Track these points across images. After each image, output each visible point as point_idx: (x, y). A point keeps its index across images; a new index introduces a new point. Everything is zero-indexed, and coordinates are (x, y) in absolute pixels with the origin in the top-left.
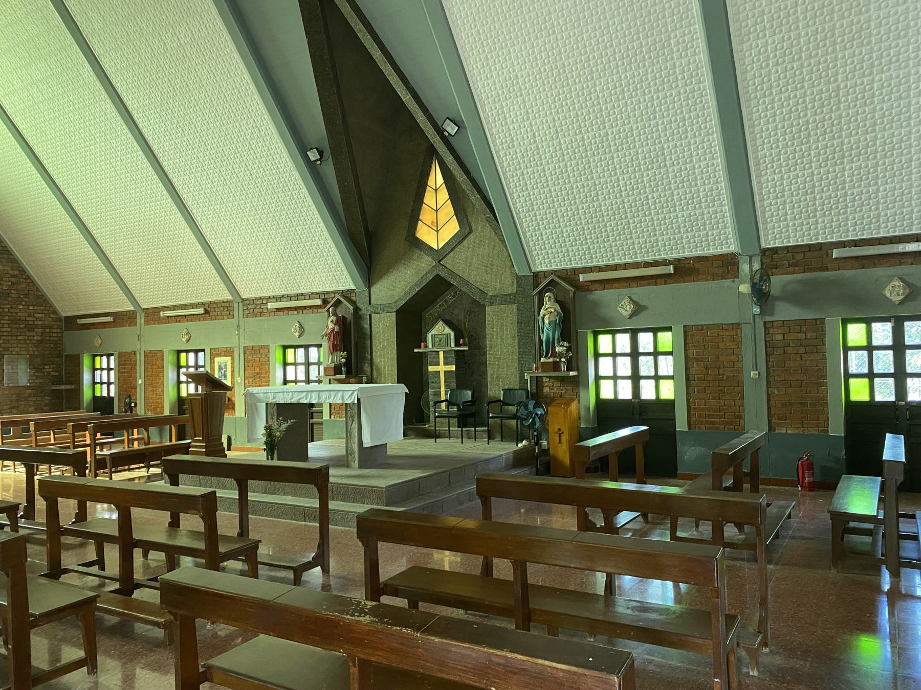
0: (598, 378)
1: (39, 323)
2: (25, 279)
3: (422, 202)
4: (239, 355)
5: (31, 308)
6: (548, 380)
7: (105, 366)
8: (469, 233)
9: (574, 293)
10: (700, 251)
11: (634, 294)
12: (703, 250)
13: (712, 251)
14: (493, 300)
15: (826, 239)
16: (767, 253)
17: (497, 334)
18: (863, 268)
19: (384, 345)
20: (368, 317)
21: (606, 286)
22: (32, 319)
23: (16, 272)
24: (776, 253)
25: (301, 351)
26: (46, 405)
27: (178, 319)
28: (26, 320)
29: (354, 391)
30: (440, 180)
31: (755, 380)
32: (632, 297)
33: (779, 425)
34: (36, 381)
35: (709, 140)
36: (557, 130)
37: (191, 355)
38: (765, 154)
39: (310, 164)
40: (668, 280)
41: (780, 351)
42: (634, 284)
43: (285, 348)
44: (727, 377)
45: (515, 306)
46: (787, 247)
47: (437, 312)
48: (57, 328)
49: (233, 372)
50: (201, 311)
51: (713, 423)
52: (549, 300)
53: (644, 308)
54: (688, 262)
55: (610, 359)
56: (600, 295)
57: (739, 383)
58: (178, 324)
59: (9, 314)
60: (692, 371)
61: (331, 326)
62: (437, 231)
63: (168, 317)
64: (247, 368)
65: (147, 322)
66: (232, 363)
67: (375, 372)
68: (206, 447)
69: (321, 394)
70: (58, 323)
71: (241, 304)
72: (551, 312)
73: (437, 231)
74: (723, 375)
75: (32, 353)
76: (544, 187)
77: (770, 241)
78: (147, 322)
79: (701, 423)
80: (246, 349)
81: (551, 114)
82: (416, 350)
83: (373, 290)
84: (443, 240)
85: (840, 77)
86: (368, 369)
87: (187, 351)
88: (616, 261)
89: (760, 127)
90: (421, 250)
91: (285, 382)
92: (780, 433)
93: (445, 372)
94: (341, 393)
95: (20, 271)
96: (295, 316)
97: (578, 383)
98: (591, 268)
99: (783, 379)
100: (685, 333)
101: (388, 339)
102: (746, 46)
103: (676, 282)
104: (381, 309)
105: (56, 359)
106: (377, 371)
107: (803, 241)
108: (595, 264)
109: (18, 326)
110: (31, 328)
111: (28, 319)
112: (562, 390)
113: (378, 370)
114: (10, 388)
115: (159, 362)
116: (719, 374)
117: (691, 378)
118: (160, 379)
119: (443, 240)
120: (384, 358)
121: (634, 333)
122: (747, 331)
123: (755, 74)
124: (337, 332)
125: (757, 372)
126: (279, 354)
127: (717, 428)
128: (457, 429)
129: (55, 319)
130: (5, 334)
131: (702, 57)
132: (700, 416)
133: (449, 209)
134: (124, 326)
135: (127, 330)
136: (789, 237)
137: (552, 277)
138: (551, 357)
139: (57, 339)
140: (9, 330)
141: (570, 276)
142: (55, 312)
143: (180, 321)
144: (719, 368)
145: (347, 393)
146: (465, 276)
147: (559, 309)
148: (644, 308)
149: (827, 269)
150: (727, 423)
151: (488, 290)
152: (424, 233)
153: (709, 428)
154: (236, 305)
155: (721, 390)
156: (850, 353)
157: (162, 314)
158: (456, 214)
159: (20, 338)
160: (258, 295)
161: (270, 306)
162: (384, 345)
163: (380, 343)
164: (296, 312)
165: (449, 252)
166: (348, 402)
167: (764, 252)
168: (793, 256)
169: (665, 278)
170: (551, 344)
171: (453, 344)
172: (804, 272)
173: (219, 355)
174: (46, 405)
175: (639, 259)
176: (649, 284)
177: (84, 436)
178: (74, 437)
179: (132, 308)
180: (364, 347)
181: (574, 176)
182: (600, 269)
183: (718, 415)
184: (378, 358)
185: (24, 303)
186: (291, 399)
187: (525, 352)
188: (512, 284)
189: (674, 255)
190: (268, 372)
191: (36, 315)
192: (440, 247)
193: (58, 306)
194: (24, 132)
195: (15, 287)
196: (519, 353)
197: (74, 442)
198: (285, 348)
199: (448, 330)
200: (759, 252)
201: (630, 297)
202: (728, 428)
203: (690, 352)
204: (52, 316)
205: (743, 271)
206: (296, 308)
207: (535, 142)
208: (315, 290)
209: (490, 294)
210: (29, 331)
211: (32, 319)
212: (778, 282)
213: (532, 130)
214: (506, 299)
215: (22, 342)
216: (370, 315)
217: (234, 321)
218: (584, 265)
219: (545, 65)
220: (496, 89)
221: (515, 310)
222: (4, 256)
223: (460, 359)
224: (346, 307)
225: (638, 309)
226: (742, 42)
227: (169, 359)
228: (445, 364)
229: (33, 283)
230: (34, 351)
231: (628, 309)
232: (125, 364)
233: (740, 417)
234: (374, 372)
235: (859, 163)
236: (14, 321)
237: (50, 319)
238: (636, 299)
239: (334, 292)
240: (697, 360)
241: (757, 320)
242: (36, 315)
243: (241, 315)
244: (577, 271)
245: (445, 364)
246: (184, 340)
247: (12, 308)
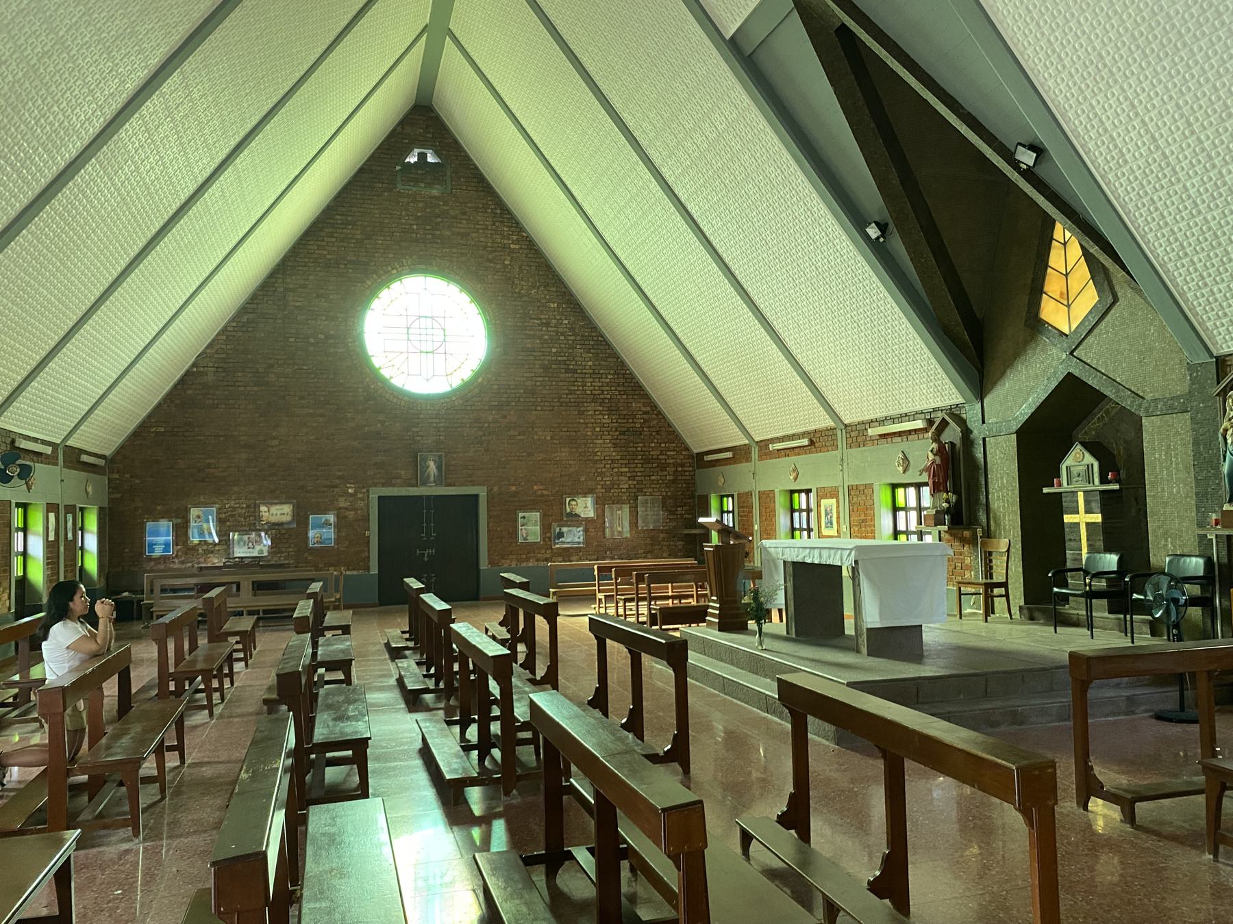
1: (671, 461)
2: (657, 415)
3: (1046, 266)
4: (843, 494)
5: (663, 445)
7: (912, 503)
19: (1002, 483)
20: (981, 442)
23: (649, 409)
26: (680, 550)
28: (658, 459)
29: (851, 550)
34: (669, 524)
36: (1188, 121)
37: (912, 491)
39: (875, 246)
43: (894, 487)
45: (1187, 416)
48: (690, 466)
49: (838, 518)
50: (805, 442)
58: (787, 458)
59: (642, 453)
61: (931, 457)
63: (778, 450)
64: (851, 513)
65: (761, 458)
66: (838, 507)
68: (720, 609)
70: (690, 461)
71: (844, 431)
73: (1069, 306)
75: (664, 494)
76: (1194, 216)
78: (761, 458)
80: (850, 488)
81: (1171, 98)
82: (1045, 490)
83: (986, 401)
87: (799, 491)
91: (896, 533)
93: (1088, 524)
94: (839, 552)
95: (651, 407)
96: (900, 445)
105: (689, 501)
106: (995, 521)
109: (650, 466)
110: (663, 467)
111: (660, 457)
114: (644, 531)
115: (772, 505)
118: (773, 525)
119: (1076, 318)
120: (1003, 501)
128: (1106, 614)
129: (687, 457)
130: (639, 474)
134: (742, 462)
135: (743, 467)
139: (690, 478)
140: (642, 470)
142: (687, 449)
143: (788, 456)
151: (1144, 391)
152: (1051, 312)
157: (771, 447)
158: (1092, 278)
159: (653, 478)
160: (861, 419)
161: (871, 432)
162: (1002, 483)
163: (997, 481)
164: (899, 439)
171: (1097, 481)
173: (825, 497)
174: (680, 550)
178: (650, 588)
179: (747, 442)
180: (977, 484)
185: (656, 441)
186: (797, 557)
187: (1207, 493)
190: (873, 519)
191: (668, 453)
195: (647, 424)
196: (1197, 494)
198: (894, 487)
199: (1089, 459)
204: (684, 453)
206: (900, 434)
207: (1158, 147)
209: (1149, 397)
213: (1147, 131)
214: (1174, 406)
215: (655, 482)
216: (984, 439)
217: (837, 453)
220: (1075, 84)
221: (1189, 422)
222: (636, 392)
223: (1108, 503)
224: (954, 430)
227: (781, 502)
237: (682, 457)
242: (668, 453)
246: (792, 477)
247: (645, 446)
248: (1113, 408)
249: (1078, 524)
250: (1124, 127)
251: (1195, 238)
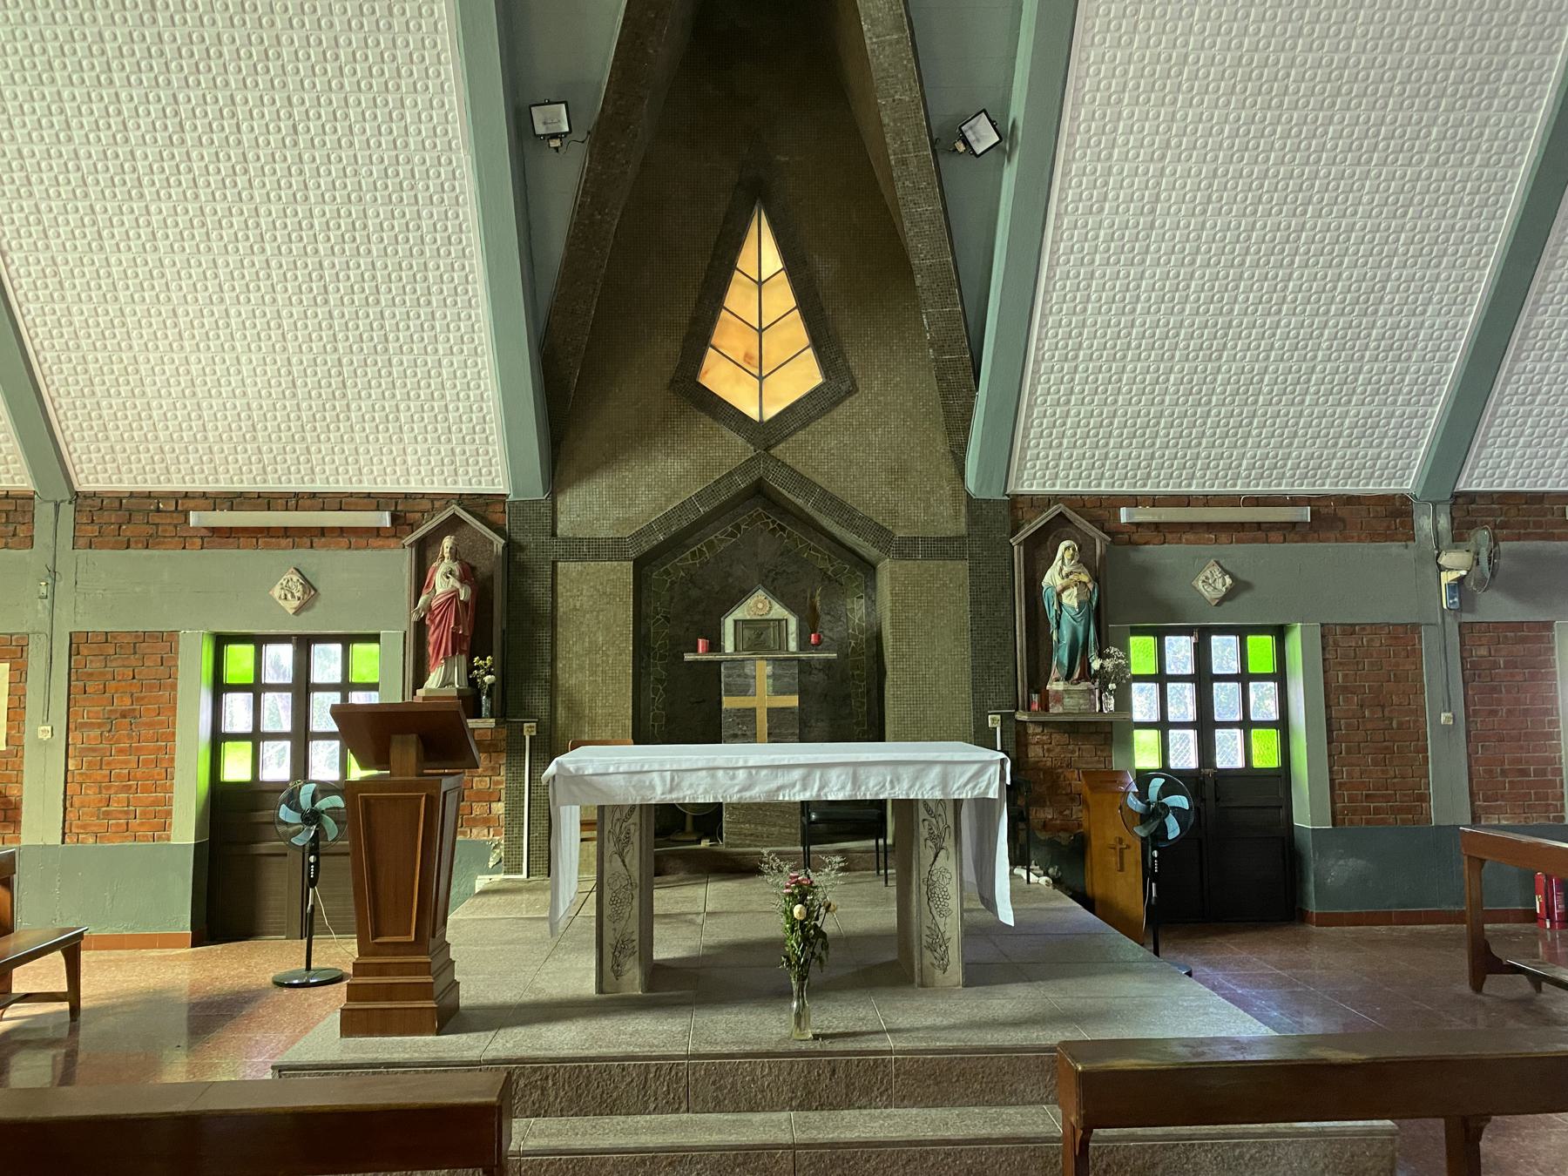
6: (1039, 730)
8: (849, 393)
13: (1372, 488)
14: (906, 549)
15: (1535, 486)
20: (548, 568)
24: (1473, 502)
29: (991, 762)
30: (772, 261)
31: (1447, 729)
32: (1221, 562)
33: (1487, 810)
43: (221, 641)
51: (1377, 811)
55: (1235, 687)
62: (761, 378)
67: (561, 712)
69: (862, 771)
71: (68, 510)
73: (761, 378)
74: (1391, 719)
79: (1354, 811)
80: (77, 643)
82: (689, 657)
83: (560, 499)
84: (777, 401)
88: (1057, 488)
90: (715, 418)
94: (937, 770)
101: (608, 629)
104: (591, 549)
112: (1073, 752)
113: (573, 707)
117: (1335, 726)
119: (777, 401)
121: (304, 644)
122: (1428, 643)
124: (465, 604)
125: (1450, 714)
127: (1383, 822)
133: (795, 332)
137: (1061, 507)
138: (1078, 681)
144: (1383, 707)
145: (958, 769)
146: (833, 489)
150: (1400, 810)
154: (43, 512)
155: (1387, 748)
165: (795, 430)
166: (966, 794)
167: (1457, 496)
169: (1289, 530)
183: (1383, 796)
188: (956, 517)
192: (767, 417)
198: (221, 641)
205: (1421, 529)
209: (900, 534)
216: (554, 564)
217: (34, 558)
231: (1219, 585)
239: (446, 498)
240: (1345, 689)
241: (1448, 619)
248: (722, 541)
249: (754, 710)
250: (227, 206)
251: (62, 376)
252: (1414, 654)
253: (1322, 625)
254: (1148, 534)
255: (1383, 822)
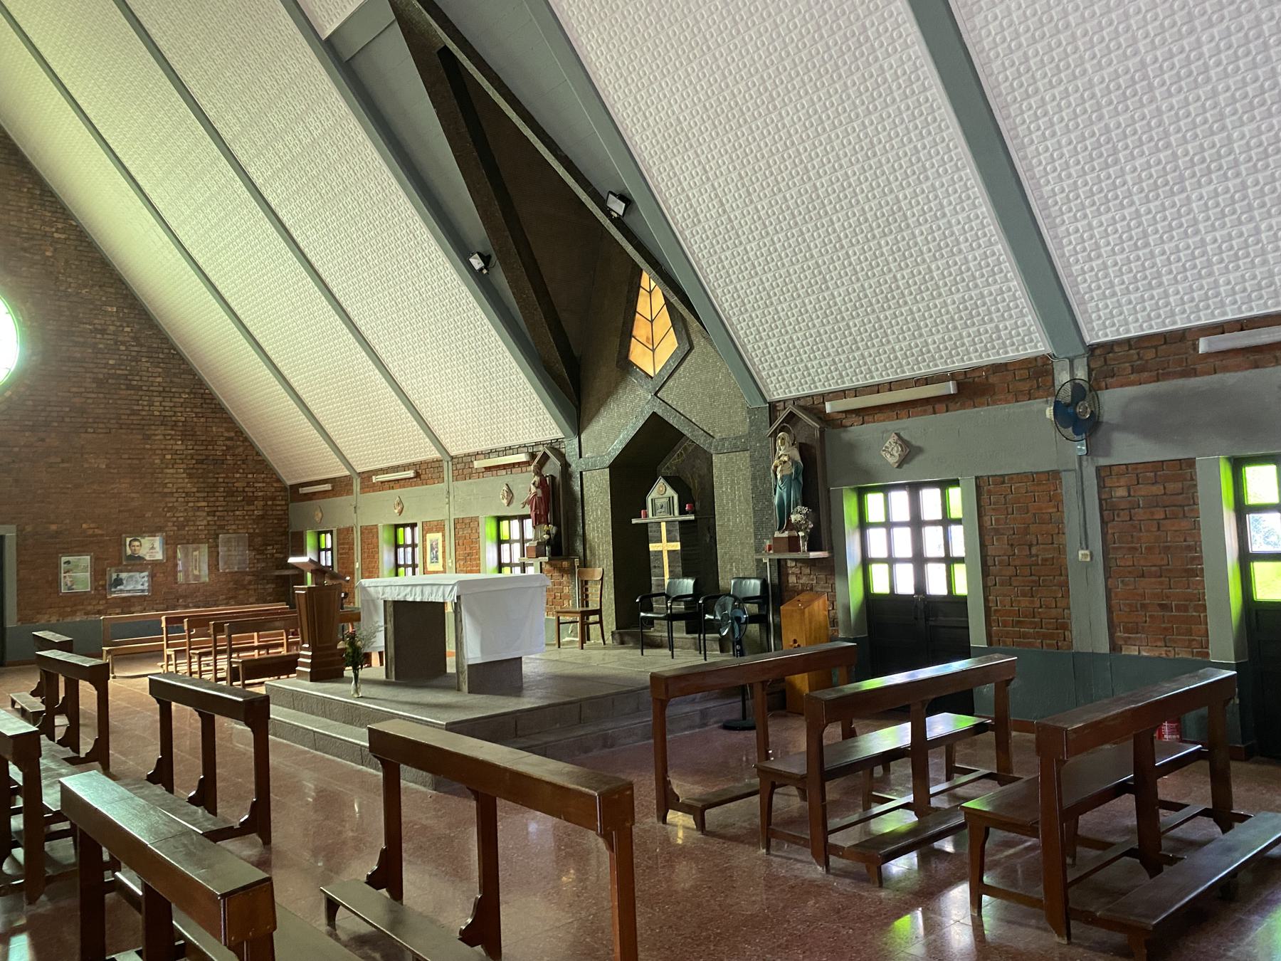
0: (866, 562)
1: (260, 494)
2: (243, 441)
3: (635, 311)
5: (250, 476)
6: (794, 564)
9: (822, 432)
10: (1031, 348)
11: (904, 429)
12: (1017, 350)
16: (1098, 352)
17: (727, 496)
18: (1257, 367)
21: (866, 418)
22: (251, 489)
23: (232, 434)
25: (515, 523)
26: (270, 594)
27: (392, 484)
32: (902, 434)
33: (1127, 640)
35: (961, 179)
38: (1053, 190)
39: (477, 275)
40: (951, 405)
41: (1125, 516)
42: (904, 412)
43: (499, 519)
44: (1042, 560)
45: (747, 454)
46: (1129, 340)
47: (676, 465)
49: (444, 552)
50: (411, 474)
51: (1025, 636)
52: (783, 444)
53: (919, 450)
54: (977, 374)
55: (883, 531)
56: (858, 432)
57: (1061, 570)
60: (991, 551)
62: (653, 350)
63: (382, 482)
67: (588, 552)
70: (282, 493)
72: (785, 462)
73: (653, 350)
74: (1037, 556)
77: (1099, 330)
80: (456, 522)
82: (634, 521)
85: (1141, 45)
86: (579, 548)
87: (404, 526)
89: (1034, 147)
91: (500, 566)
92: (1129, 656)
97: (833, 567)
98: (844, 391)
99: (1131, 563)
100: (978, 487)
102: (978, 20)
103: (963, 407)
107: (1199, 319)
108: (847, 385)
110: (250, 501)
111: (247, 489)
112: (813, 580)
116: (1031, 555)
117: (990, 562)
119: (660, 362)
123: (1003, 64)
125: (1087, 552)
126: (488, 529)
127: (1031, 645)
130: (220, 509)
131: (918, 49)
132: (1005, 624)
136: (1127, 323)
138: (786, 529)
140: (224, 503)
141: (812, 406)
142: (279, 480)
143: (393, 488)
144: (1030, 546)
147: (798, 458)
148: (919, 450)
149: (1194, 373)
150: (1045, 636)
151: (714, 431)
152: (639, 355)
153: (1019, 644)
154: (445, 464)
156: (1251, 518)
159: (237, 513)
161: (477, 464)
167: (1092, 349)
168: (1138, 354)
170: (784, 511)
171: (676, 512)
172: (1158, 380)
173: (431, 531)
174: (270, 594)
175: (908, 374)
176: (925, 413)
177: (252, 637)
178: (230, 640)
179: (347, 473)
181: (967, 240)
182: (856, 392)
183: (1031, 623)
184: (592, 534)
187: (762, 523)
189: (957, 365)
190: (478, 553)
193: (281, 472)
194: (203, 267)
197: (216, 646)
199: (670, 492)
200: (1083, 352)
201: (898, 434)
202: (1047, 645)
203: (987, 518)
204: (275, 485)
206: (504, 467)
208: (522, 442)
210: (248, 504)
211: (251, 489)
212: (1113, 400)
216: (581, 473)
218: (833, 387)
219: (818, 90)
225: (910, 452)
226: (971, 16)
227: (384, 537)
228: (668, 541)
229: (252, 446)
230: (254, 529)
232: (343, 544)
233: (1065, 627)
234: (588, 552)
235: (1212, 187)
236: (231, 493)
238: (906, 437)
240: (997, 531)
241: (1085, 463)
243: (451, 479)
244: (824, 397)
245: (668, 541)
247: (227, 477)
249: (661, 552)
252: (1056, 500)
253: (977, 478)
254: (853, 418)
255: (1031, 645)
